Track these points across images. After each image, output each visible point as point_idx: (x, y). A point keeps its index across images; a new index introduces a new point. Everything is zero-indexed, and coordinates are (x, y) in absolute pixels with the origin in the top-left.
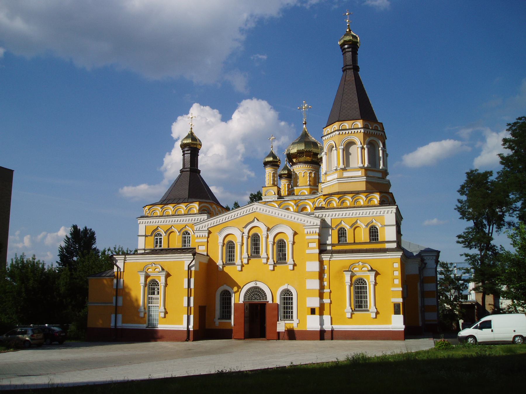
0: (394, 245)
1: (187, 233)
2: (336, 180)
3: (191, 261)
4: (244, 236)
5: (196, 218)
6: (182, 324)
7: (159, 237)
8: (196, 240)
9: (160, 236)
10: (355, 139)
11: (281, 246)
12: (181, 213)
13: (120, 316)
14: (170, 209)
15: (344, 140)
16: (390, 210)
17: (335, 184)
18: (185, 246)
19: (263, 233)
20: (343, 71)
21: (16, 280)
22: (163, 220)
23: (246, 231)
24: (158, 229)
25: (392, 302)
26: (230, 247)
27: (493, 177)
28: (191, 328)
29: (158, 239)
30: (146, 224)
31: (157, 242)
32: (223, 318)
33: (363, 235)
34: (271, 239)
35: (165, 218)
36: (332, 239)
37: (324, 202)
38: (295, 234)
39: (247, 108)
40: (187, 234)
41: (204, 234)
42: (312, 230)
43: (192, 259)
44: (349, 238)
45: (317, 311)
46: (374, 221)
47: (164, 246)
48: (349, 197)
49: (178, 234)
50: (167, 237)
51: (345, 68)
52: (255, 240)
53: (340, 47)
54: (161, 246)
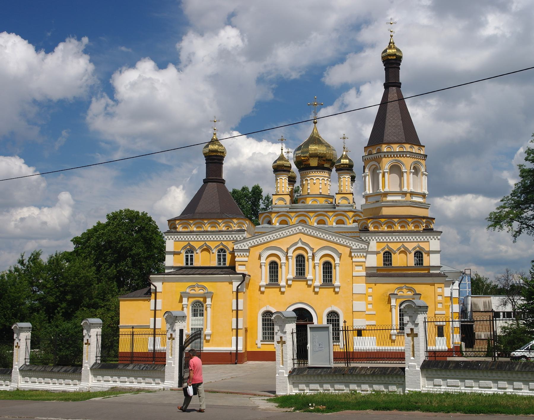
11: (328, 268)
13: (158, 338)
26: (274, 267)
31: (187, 259)
33: (411, 261)
36: (387, 263)
52: (301, 261)
54: (192, 264)
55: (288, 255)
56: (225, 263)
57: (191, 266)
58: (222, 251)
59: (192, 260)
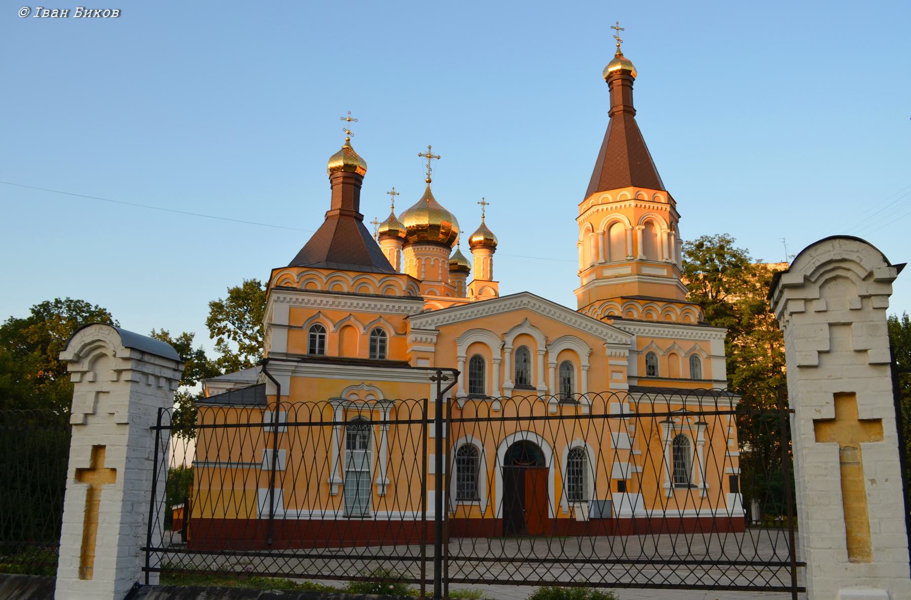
0: (724, 387)
1: (379, 332)
2: (637, 276)
3: (448, 385)
4: (505, 349)
5: (403, 306)
6: (286, 506)
7: (318, 334)
8: (609, 361)
9: (320, 332)
10: (654, 217)
12: (369, 293)
14: (321, 279)
15: (644, 217)
16: (719, 334)
17: (633, 282)
18: (375, 356)
19: (537, 346)
20: (610, 116)
21: (865, 558)
22: (331, 300)
23: (509, 340)
24: (319, 317)
25: (728, 474)
26: (477, 365)
27: (204, 349)
28: (429, 517)
29: (318, 337)
30: (291, 304)
31: (313, 343)
32: (469, 497)
33: (682, 369)
34: (552, 358)
35: (336, 297)
37: (693, 302)
38: (591, 355)
39: (420, 156)
40: (379, 334)
41: (429, 337)
42: (618, 351)
44: (662, 372)
45: (614, 486)
46: (698, 348)
47: (330, 350)
48: (658, 307)
49: (362, 331)
50: (337, 335)
51: (611, 112)
53: (605, 80)
55: (505, 347)
56: (323, 350)
57: (321, 356)
58: (315, 332)
59: (322, 344)
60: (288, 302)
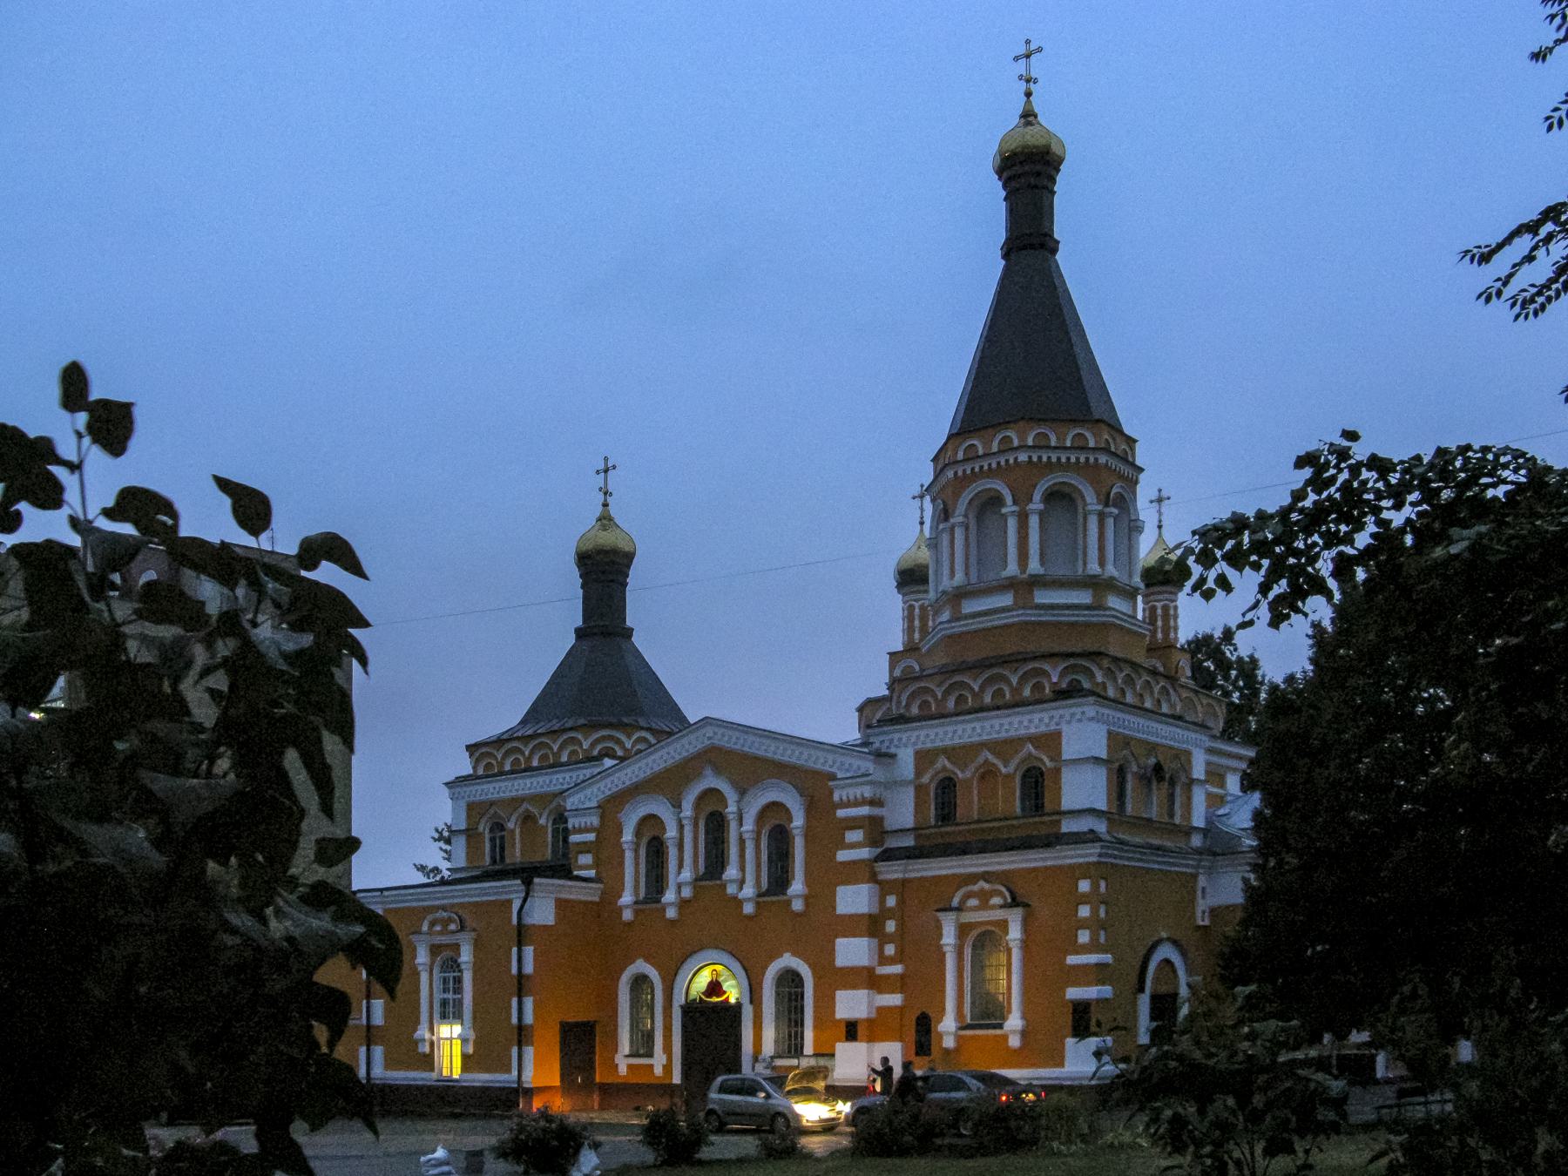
6: (387, 1066)
11: (780, 842)
28: (529, 1080)
42: (583, 820)
43: (523, 895)
45: (861, 1031)
60: (463, 797)
